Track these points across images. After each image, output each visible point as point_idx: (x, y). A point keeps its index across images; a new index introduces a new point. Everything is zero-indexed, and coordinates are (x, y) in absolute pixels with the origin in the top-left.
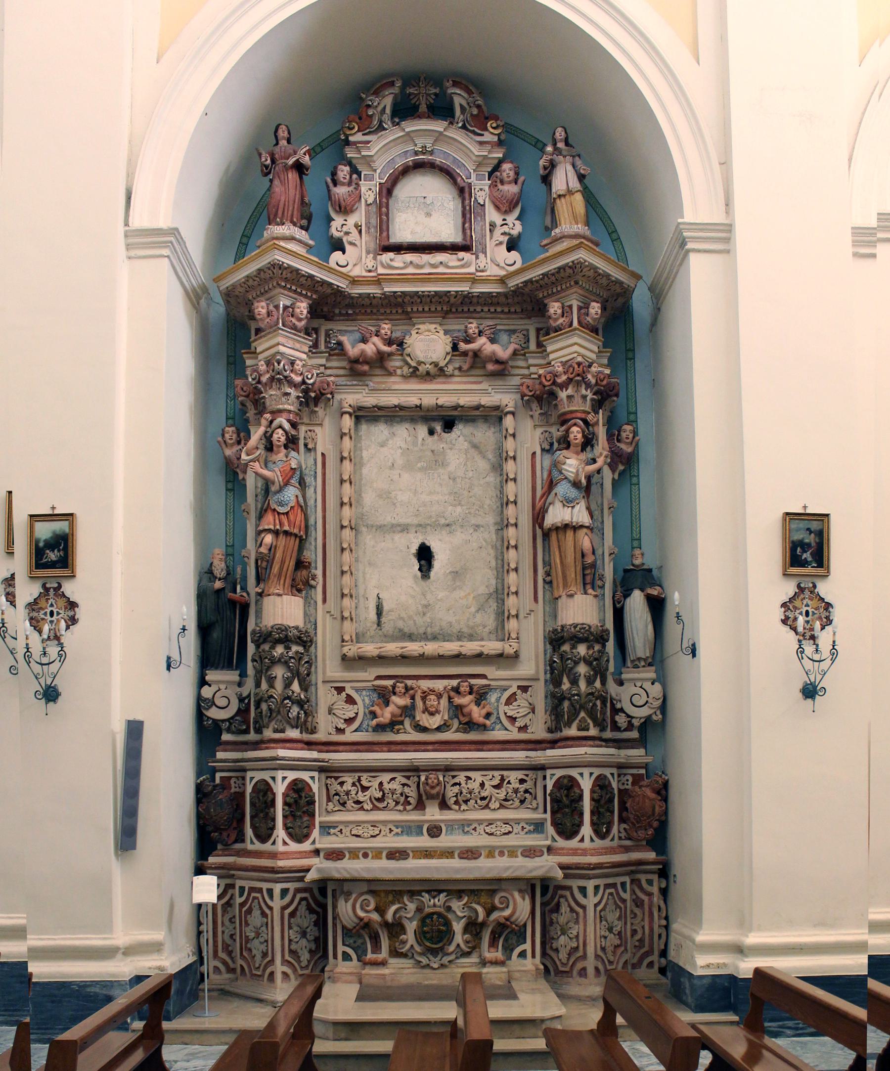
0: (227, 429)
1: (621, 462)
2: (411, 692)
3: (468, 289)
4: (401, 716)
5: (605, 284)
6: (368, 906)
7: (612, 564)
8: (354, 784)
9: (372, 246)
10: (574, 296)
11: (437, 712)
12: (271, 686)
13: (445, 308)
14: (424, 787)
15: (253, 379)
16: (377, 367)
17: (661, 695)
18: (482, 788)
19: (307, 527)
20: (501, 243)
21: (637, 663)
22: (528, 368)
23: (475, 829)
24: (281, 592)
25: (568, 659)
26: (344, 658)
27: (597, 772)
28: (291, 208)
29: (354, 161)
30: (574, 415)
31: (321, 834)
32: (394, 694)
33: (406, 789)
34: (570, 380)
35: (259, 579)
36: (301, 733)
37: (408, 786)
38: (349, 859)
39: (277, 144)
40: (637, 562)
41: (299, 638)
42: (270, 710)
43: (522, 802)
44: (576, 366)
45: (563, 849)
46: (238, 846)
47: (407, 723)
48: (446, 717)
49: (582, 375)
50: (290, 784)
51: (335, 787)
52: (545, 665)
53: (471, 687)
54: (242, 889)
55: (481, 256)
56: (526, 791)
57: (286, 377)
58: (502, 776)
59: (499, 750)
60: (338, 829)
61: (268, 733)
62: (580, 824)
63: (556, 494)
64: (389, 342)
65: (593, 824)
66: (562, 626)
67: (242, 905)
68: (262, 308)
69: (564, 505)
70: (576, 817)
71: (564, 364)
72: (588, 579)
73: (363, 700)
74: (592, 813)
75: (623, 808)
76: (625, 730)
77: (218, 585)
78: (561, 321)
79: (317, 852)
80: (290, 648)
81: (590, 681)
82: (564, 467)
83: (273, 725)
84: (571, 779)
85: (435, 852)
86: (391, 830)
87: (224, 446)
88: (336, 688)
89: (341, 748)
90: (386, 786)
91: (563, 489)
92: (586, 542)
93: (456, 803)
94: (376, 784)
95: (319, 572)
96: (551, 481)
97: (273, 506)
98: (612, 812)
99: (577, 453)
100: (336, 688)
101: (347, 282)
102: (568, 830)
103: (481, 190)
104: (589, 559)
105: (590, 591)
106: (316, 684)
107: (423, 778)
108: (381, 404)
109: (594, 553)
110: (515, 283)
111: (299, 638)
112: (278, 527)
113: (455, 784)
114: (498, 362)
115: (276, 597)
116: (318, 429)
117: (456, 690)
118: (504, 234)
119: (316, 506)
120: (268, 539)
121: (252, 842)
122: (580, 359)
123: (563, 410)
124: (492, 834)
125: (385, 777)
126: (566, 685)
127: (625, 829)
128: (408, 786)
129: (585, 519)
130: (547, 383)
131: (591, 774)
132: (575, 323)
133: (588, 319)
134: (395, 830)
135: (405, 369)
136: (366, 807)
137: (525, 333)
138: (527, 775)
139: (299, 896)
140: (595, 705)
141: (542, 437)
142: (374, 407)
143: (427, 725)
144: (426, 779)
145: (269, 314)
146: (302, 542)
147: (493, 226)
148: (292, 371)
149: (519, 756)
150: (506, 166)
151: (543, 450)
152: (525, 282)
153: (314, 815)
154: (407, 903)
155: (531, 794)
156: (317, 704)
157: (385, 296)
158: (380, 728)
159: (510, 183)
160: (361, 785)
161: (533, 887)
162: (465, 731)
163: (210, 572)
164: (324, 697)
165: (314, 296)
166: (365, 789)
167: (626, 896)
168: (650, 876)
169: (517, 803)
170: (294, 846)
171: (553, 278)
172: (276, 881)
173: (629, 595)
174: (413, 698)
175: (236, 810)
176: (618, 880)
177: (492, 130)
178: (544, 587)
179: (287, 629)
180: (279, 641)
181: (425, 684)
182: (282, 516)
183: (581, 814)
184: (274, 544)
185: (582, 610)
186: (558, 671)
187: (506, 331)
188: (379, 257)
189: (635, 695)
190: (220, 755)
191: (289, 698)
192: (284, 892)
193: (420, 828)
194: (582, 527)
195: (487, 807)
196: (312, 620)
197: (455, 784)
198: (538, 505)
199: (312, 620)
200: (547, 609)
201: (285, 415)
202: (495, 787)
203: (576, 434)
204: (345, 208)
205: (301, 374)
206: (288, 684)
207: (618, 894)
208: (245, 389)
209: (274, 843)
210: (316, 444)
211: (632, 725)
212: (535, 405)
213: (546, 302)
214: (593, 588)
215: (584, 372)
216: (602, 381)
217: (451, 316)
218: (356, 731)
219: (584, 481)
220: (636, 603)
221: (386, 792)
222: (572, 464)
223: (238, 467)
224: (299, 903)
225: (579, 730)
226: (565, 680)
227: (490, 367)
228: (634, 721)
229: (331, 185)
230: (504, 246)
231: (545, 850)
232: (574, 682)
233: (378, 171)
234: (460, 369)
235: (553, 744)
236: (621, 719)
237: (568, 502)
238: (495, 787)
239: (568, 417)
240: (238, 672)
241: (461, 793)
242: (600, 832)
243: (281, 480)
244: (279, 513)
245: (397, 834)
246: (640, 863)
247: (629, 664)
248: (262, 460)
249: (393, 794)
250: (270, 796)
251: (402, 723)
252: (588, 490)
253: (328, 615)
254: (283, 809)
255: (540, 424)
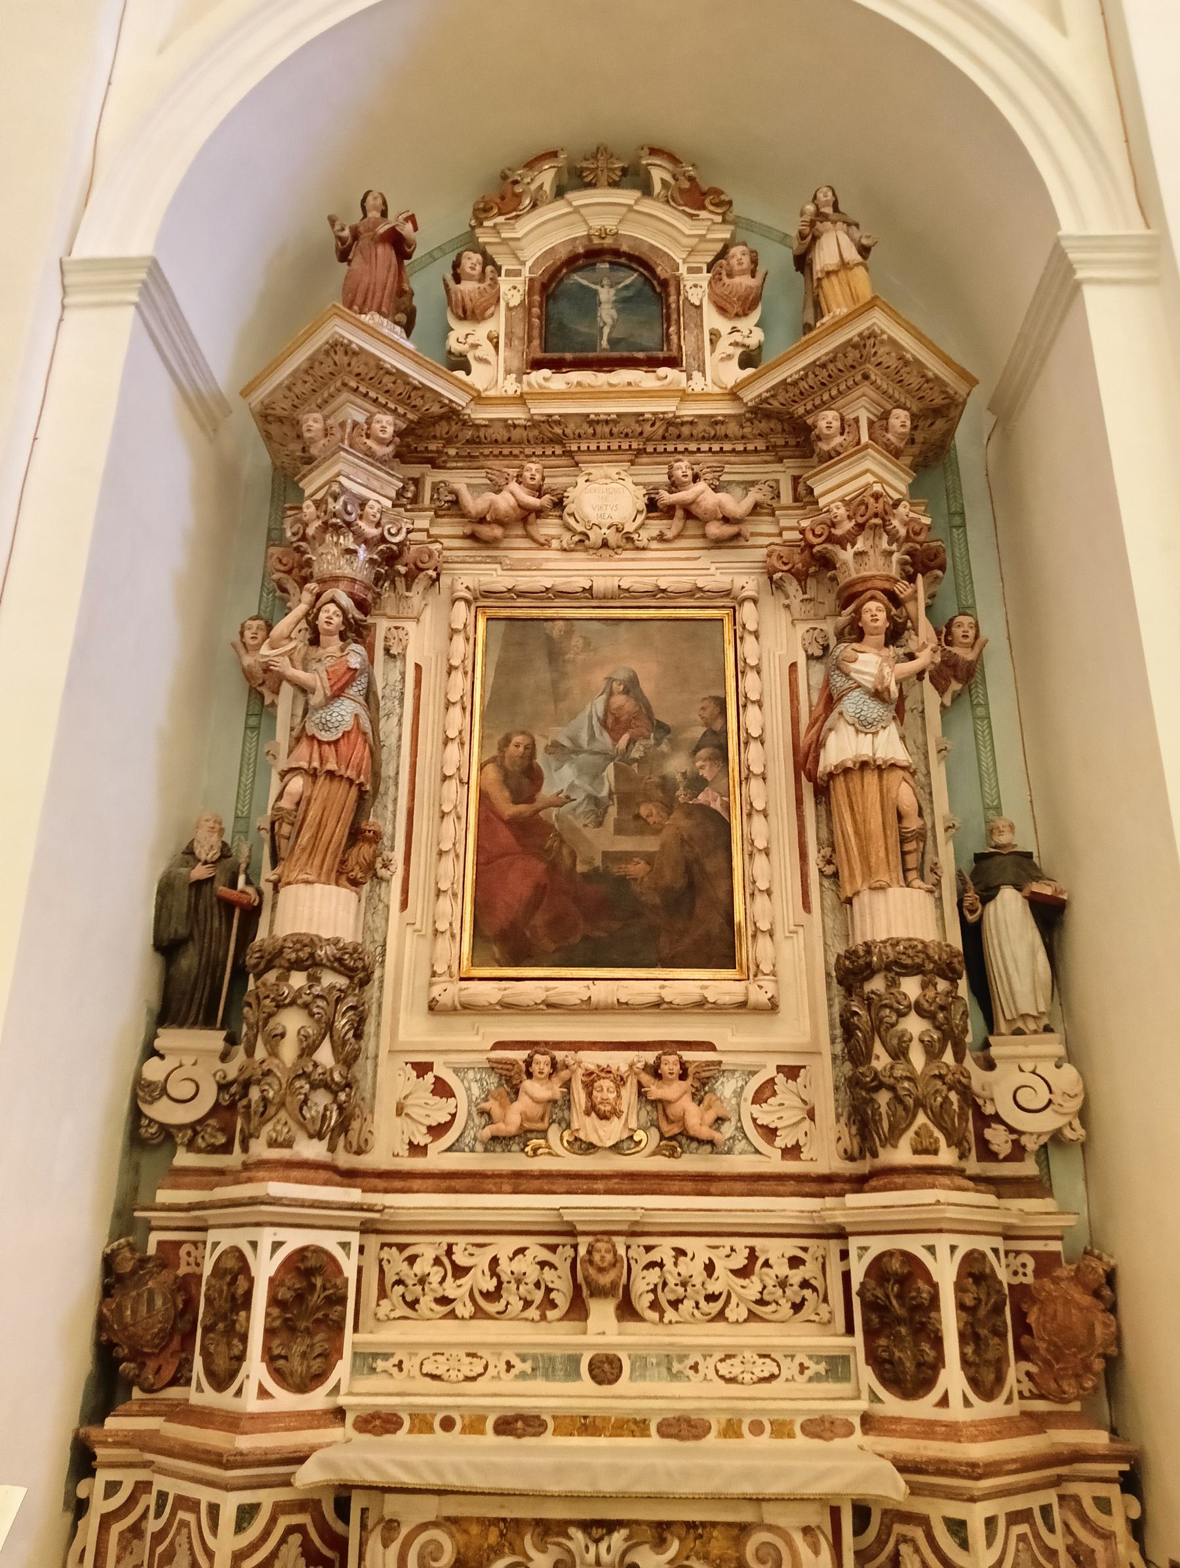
0: (250, 622)
1: (956, 678)
2: (564, 1074)
3: (674, 409)
4: (542, 1119)
5: (915, 386)
6: (435, 1560)
7: (951, 845)
8: (437, 1261)
9: (516, 363)
10: (863, 401)
11: (616, 1113)
12: (274, 1053)
13: (635, 446)
14: (584, 1270)
15: (294, 534)
16: (517, 536)
17: (1079, 1089)
18: (710, 1275)
19: (376, 775)
20: (730, 357)
21: (1020, 1024)
22: (780, 535)
23: (695, 1368)
24: (311, 878)
25: (886, 1006)
26: (433, 1007)
27: (966, 1244)
28: (378, 294)
29: (490, 250)
30: (869, 584)
31: (355, 1371)
32: (530, 1075)
33: (548, 1274)
34: (861, 527)
35: (275, 860)
36: (332, 1149)
37: (552, 1266)
38: (411, 1431)
39: (365, 216)
40: (1003, 839)
41: (340, 960)
42: (265, 1100)
43: (797, 1307)
44: (872, 500)
45: (898, 1420)
46: (174, 1393)
47: (554, 1133)
48: (633, 1124)
49: (884, 516)
50: (333, 1259)
51: (397, 1265)
52: (832, 1027)
53: (684, 1066)
54: (162, 1496)
55: (697, 375)
56: (805, 1284)
57: (349, 524)
58: (752, 1250)
59: (742, 1195)
60: (395, 1360)
61: (260, 1149)
62: (939, 1362)
63: (841, 713)
64: (539, 491)
65: (965, 1362)
66: (868, 947)
67: (158, 1537)
68: (315, 421)
69: (857, 731)
70: (926, 1347)
71: (847, 504)
72: (912, 861)
73: (468, 1089)
74: (963, 1337)
75: (1022, 1327)
76: (1007, 1159)
77: (200, 872)
78: (839, 440)
79: (339, 1414)
80: (318, 980)
81: (932, 1052)
82: (852, 666)
83: (267, 1130)
84: (909, 1258)
85: (606, 1419)
86: (509, 1366)
87: (243, 651)
88: (415, 1065)
89: (416, 1184)
90: (504, 1267)
91: (853, 704)
92: (905, 795)
93: (655, 1305)
94: (482, 1261)
95: (398, 856)
96: (830, 697)
97: (311, 729)
98: (1003, 1336)
99: (878, 647)
100: (415, 1065)
101: (469, 398)
102: (911, 1378)
103: (696, 286)
104: (913, 823)
105: (917, 883)
106: (376, 1057)
107: (582, 1251)
108: (522, 587)
109: (920, 815)
110: (756, 393)
111: (340, 960)
112: (316, 764)
113: (651, 1265)
114: (726, 520)
115: (302, 886)
116: (410, 626)
117: (655, 1071)
118: (736, 344)
119: (399, 747)
120: (297, 784)
121: (200, 1389)
122: (877, 488)
123: (848, 579)
124: (732, 1380)
125: (504, 1246)
126: (881, 1060)
127: (1028, 1374)
128: (552, 1266)
129: (901, 755)
130: (815, 541)
131: (953, 1248)
132: (865, 438)
133: (889, 436)
134: (519, 1366)
135: (567, 536)
136: (460, 1310)
137: (774, 484)
138: (805, 1249)
139: (284, 1522)
140: (946, 1099)
141: (807, 636)
142: (509, 590)
143: (596, 1141)
144: (589, 1252)
145: (327, 432)
146: (364, 799)
147: (715, 336)
148: (361, 517)
149: (791, 1208)
150: (737, 251)
151: (810, 657)
152: (773, 388)
153: (339, 1327)
154: (532, 1552)
155: (815, 1289)
156: (374, 1095)
157: (534, 424)
158: (498, 1142)
159: (743, 273)
160: (453, 1263)
161: (835, 1513)
162: (672, 1154)
163: (190, 851)
164: (389, 1082)
165: (410, 416)
166: (460, 1271)
167: (1056, 1541)
168: (1102, 1490)
169: (786, 1309)
170: (285, 1400)
171: (825, 373)
172: (228, 1487)
173: (993, 897)
174: (567, 1084)
175: (182, 1313)
176: (1033, 1501)
177: (711, 208)
178: (821, 885)
179: (312, 942)
180: (297, 965)
181: (592, 1059)
182: (326, 748)
183: (937, 1342)
184: (307, 794)
185: (905, 915)
186: (858, 1030)
187: (739, 483)
188: (525, 377)
189: (1022, 1083)
190: (164, 1196)
191: (305, 1075)
192: (246, 1514)
193: (574, 1360)
194: (893, 766)
195: (721, 1316)
196: (378, 937)
197: (651, 1265)
198: (804, 740)
199: (378, 937)
200: (829, 923)
201: (343, 584)
202: (737, 1273)
203: (875, 613)
204: (473, 312)
205: (378, 525)
206: (308, 1049)
207: (1037, 1536)
208: (284, 561)
209: (239, 1393)
210: (405, 649)
211: (1023, 1149)
212: (792, 587)
213: (810, 421)
214: (922, 878)
215: (886, 513)
216: (917, 534)
217: (645, 460)
218: (449, 1149)
219: (894, 689)
220: (1009, 914)
221: (505, 1278)
222: (869, 663)
223: (263, 683)
224: (283, 1540)
225: (916, 1152)
226: (878, 1048)
227: (715, 529)
228: (1024, 1140)
229: (451, 283)
230: (736, 361)
231: (856, 1421)
232: (899, 1053)
233: (529, 264)
234: (661, 538)
235: (860, 1183)
236: (997, 1138)
237: (864, 726)
238: (737, 1273)
239: (859, 588)
240: (224, 1033)
241: (665, 1284)
242: (984, 1383)
243: (327, 684)
244: (320, 743)
245: (523, 1375)
246: (1079, 1456)
247: (1003, 1027)
248: (297, 657)
249: (519, 1282)
250: (242, 1283)
251: (543, 1134)
252: (899, 713)
253: (409, 929)
254: (268, 1315)
255: (803, 616)
